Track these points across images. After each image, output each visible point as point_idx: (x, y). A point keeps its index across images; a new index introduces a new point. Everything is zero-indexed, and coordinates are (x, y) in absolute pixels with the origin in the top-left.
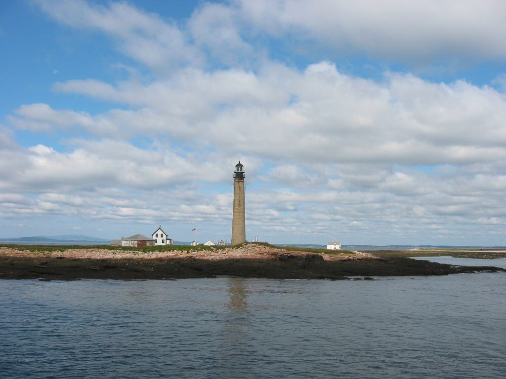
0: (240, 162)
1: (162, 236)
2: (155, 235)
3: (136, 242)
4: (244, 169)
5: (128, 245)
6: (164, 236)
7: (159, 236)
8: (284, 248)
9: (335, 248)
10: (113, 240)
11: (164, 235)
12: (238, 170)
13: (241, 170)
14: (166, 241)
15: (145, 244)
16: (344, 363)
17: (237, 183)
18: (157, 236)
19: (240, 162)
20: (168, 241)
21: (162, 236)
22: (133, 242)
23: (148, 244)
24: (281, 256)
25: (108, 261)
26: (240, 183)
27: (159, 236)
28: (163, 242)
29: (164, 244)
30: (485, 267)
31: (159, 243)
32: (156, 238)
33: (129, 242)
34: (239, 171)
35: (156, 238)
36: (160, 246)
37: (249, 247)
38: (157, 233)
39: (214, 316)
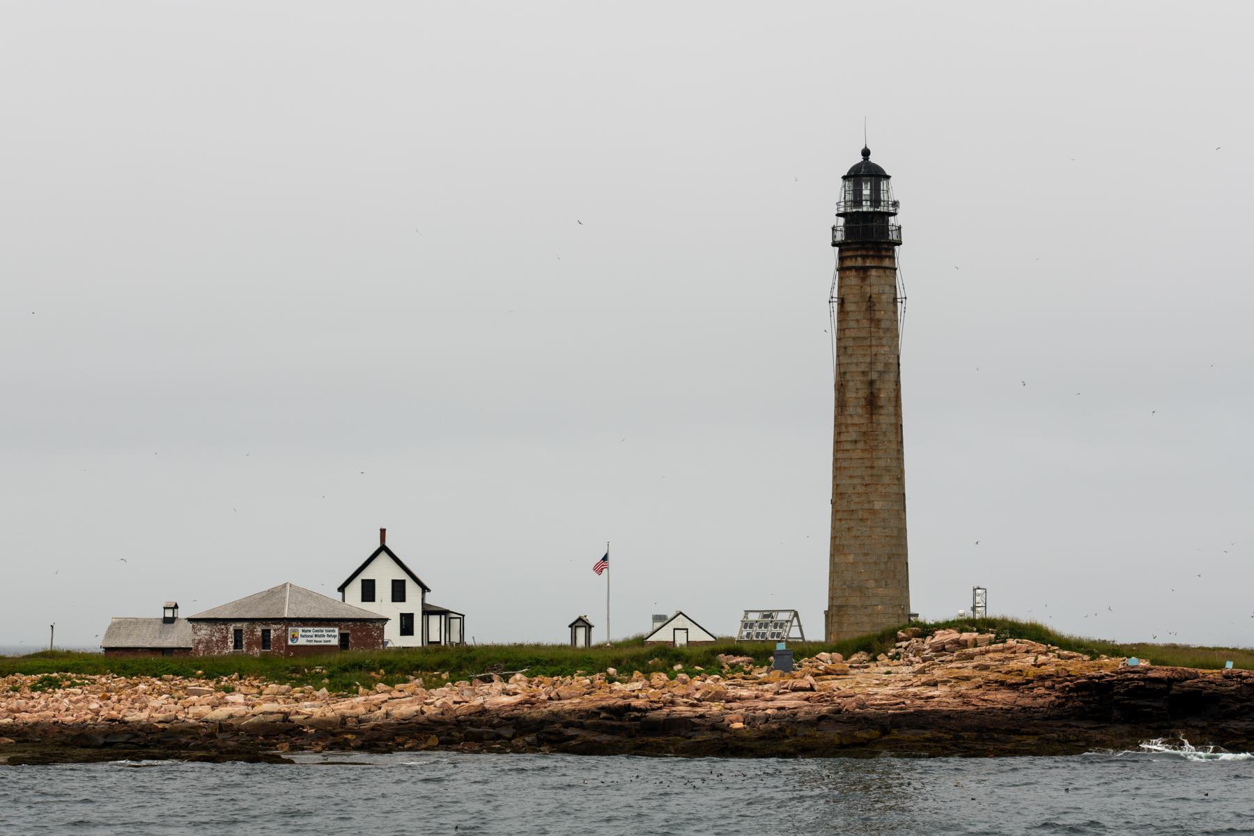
0: (866, 153)
1: (398, 592)
6: (412, 590)
7: (383, 590)
13: (876, 200)
19: (866, 153)
21: (398, 592)
27: (383, 590)
29: (414, 641)
35: (404, 608)
38: (367, 575)
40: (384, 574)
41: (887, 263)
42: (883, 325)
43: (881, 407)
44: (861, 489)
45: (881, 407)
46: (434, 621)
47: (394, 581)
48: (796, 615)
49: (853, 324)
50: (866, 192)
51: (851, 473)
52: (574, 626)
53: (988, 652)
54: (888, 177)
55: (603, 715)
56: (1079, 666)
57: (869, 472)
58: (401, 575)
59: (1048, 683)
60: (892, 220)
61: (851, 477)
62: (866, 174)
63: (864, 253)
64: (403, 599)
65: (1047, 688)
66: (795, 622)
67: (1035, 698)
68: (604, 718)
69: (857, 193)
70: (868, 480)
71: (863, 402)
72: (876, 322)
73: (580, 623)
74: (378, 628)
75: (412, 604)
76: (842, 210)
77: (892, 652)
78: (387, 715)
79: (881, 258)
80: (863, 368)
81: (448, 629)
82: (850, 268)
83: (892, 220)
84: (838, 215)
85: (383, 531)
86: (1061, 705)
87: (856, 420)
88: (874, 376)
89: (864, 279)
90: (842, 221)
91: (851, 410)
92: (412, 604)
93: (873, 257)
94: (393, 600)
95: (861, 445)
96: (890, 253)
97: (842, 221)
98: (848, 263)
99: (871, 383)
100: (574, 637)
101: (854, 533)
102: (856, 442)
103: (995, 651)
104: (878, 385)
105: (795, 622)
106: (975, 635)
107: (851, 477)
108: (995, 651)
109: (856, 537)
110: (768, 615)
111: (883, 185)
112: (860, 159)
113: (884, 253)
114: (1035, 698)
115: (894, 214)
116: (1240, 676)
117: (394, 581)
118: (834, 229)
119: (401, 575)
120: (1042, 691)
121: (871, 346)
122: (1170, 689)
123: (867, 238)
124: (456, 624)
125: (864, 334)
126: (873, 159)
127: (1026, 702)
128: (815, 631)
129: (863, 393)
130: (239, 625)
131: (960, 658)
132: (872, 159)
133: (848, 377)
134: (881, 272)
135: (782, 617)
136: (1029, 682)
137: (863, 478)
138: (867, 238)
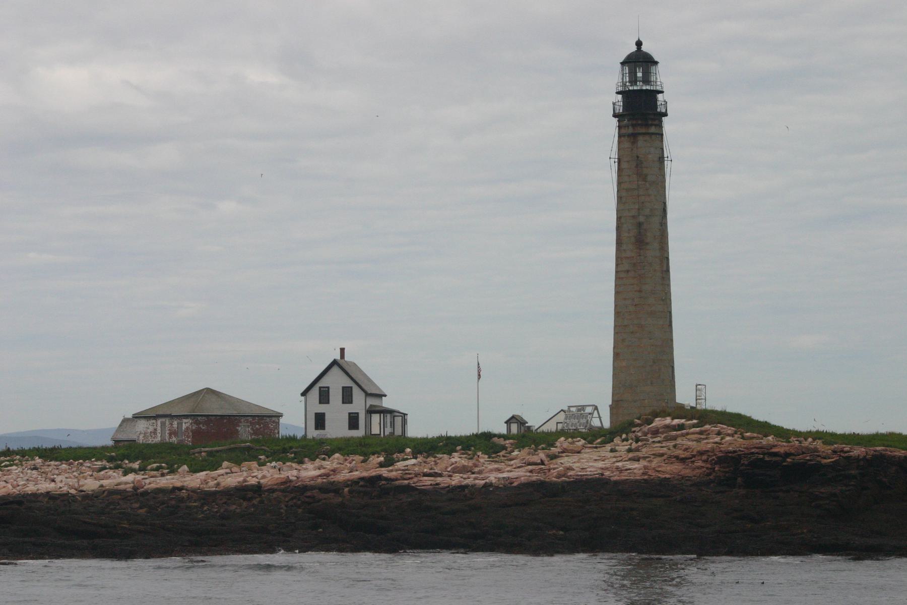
0: (639, 44)
1: (347, 396)
2: (315, 392)
3: (186, 424)
4: (666, 78)
5: (158, 439)
6: (357, 395)
7: (336, 396)
8: (757, 448)
9: (218, 484)
11: (356, 392)
12: (634, 81)
13: (646, 80)
14: (368, 424)
19: (639, 44)
21: (347, 396)
23: (245, 432)
25: (466, 491)
26: (641, 141)
27: (336, 396)
28: (353, 421)
29: (360, 433)
30: (891, 435)
32: (322, 408)
33: (163, 424)
34: (639, 86)
35: (322, 408)
36: (348, 441)
37: (656, 432)
38: (323, 383)
40: (336, 382)
41: (653, 130)
42: (649, 178)
43: (647, 244)
45: (647, 244)
46: (376, 418)
47: (343, 388)
48: (596, 408)
50: (639, 75)
52: (508, 422)
53: (688, 434)
54: (656, 63)
55: (361, 483)
56: (732, 441)
58: (348, 383)
59: (705, 457)
60: (660, 97)
61: (625, 299)
62: (640, 61)
63: (634, 122)
64: (351, 402)
65: (704, 461)
66: (596, 414)
67: (694, 469)
68: (361, 486)
69: (633, 74)
72: (644, 178)
73: (514, 420)
74: (274, 422)
75: (359, 404)
76: (620, 89)
77: (624, 436)
78: (218, 484)
79: (647, 126)
81: (393, 425)
82: (624, 136)
83: (660, 97)
84: (618, 93)
85: (342, 350)
86: (709, 474)
87: (629, 254)
88: (642, 219)
89: (633, 143)
90: (620, 97)
91: (624, 247)
92: (359, 404)
93: (641, 125)
96: (657, 122)
97: (620, 97)
99: (640, 225)
100: (509, 429)
102: (628, 271)
103: (693, 433)
105: (596, 414)
106: (683, 421)
107: (625, 299)
108: (693, 433)
110: (583, 408)
111: (653, 69)
113: (650, 122)
114: (694, 469)
115: (662, 92)
116: (842, 451)
118: (614, 104)
119: (348, 383)
120: (700, 464)
121: (638, 196)
122: (785, 461)
123: (640, 113)
124: (398, 420)
126: (644, 48)
127: (687, 472)
128: (604, 420)
130: (163, 420)
131: (667, 439)
132: (644, 48)
134: (647, 138)
135: (589, 410)
136: (694, 456)
138: (640, 113)
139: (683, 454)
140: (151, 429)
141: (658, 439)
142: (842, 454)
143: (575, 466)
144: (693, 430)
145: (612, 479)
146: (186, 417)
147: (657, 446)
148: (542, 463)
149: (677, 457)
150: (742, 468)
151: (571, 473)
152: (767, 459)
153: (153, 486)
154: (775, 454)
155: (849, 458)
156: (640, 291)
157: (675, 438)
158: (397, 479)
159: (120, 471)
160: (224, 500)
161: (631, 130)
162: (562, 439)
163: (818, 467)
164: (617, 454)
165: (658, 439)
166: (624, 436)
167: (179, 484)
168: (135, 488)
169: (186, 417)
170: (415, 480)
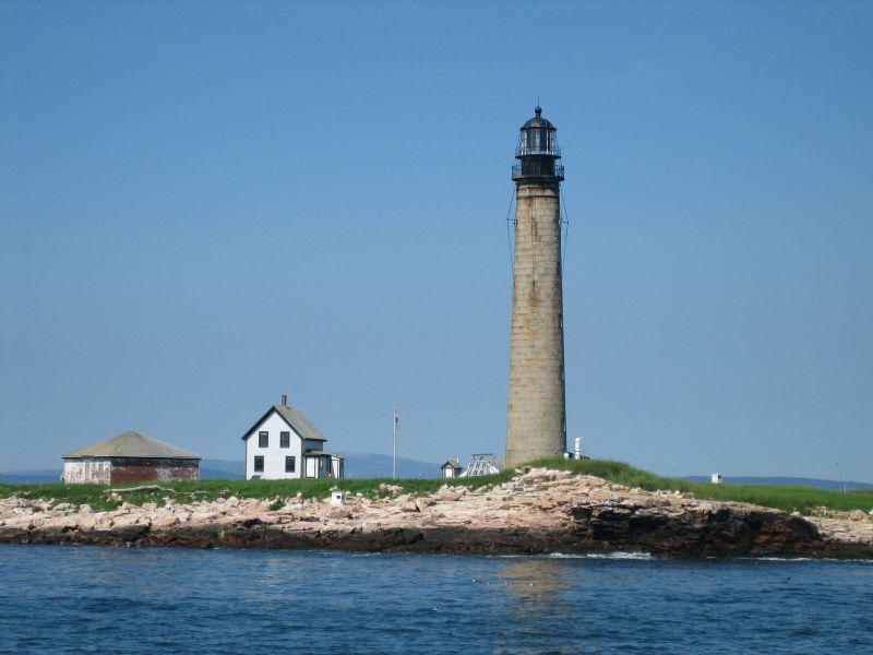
0: (538, 111)
1: (285, 440)
4: (562, 143)
7: (274, 440)
10: (851, 484)
12: (530, 145)
15: (595, 533)
16: (425, 610)
17: (523, 206)
18: (264, 441)
19: (538, 111)
20: (312, 464)
21: (285, 440)
22: (97, 464)
24: (603, 516)
26: (537, 202)
27: (274, 440)
28: (290, 466)
29: (296, 475)
31: (275, 471)
34: (536, 152)
35: (261, 452)
37: (530, 482)
38: (263, 428)
39: (319, 598)
44: (524, 363)
47: (282, 433)
49: (522, 239)
51: (518, 351)
54: (555, 129)
55: (239, 527)
57: (531, 349)
59: (563, 508)
60: (557, 161)
62: (541, 128)
70: (529, 356)
71: (527, 297)
80: (529, 271)
84: (518, 157)
86: (564, 525)
87: (523, 311)
88: (536, 278)
89: (529, 205)
94: (260, 446)
95: (525, 330)
96: (553, 186)
98: (521, 194)
101: (519, 396)
102: (521, 327)
103: (563, 484)
104: (538, 284)
108: (563, 484)
109: (520, 399)
112: (534, 115)
117: (282, 433)
119: (286, 428)
125: (529, 246)
129: (528, 290)
131: (539, 489)
132: (543, 115)
133: (518, 279)
137: (526, 354)
139: (546, 504)
140: (77, 470)
141: (531, 489)
142: (689, 509)
143: (447, 514)
144: (564, 481)
145: (224, 520)
146: (106, 458)
147: (529, 494)
148: (418, 510)
149: (540, 507)
150: (592, 520)
151: (442, 520)
152: (616, 511)
153: (51, 525)
154: (624, 507)
155: (693, 512)
156: (533, 347)
157: (546, 488)
158: (271, 524)
159: (29, 511)
160: (844, 625)
161: (527, 193)
162: (446, 486)
163: (664, 521)
164: (493, 502)
165: (531, 489)
166: (504, 485)
167: (73, 524)
168: (31, 527)
169: (106, 458)
170: (292, 524)
